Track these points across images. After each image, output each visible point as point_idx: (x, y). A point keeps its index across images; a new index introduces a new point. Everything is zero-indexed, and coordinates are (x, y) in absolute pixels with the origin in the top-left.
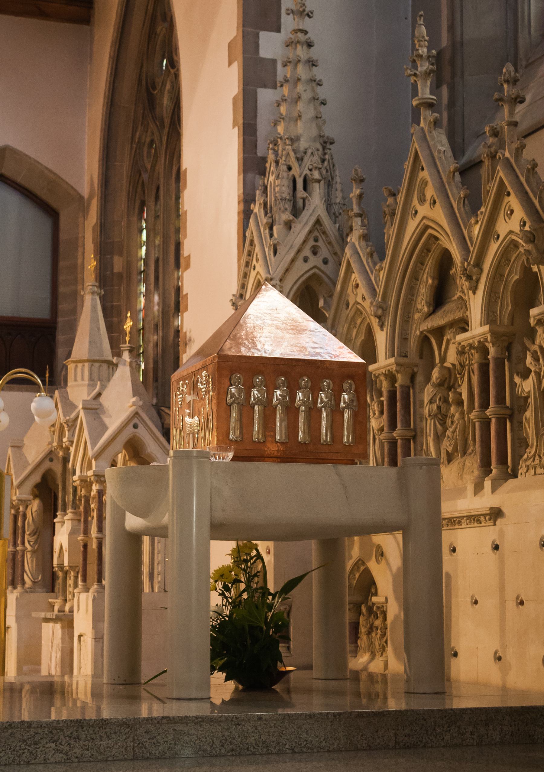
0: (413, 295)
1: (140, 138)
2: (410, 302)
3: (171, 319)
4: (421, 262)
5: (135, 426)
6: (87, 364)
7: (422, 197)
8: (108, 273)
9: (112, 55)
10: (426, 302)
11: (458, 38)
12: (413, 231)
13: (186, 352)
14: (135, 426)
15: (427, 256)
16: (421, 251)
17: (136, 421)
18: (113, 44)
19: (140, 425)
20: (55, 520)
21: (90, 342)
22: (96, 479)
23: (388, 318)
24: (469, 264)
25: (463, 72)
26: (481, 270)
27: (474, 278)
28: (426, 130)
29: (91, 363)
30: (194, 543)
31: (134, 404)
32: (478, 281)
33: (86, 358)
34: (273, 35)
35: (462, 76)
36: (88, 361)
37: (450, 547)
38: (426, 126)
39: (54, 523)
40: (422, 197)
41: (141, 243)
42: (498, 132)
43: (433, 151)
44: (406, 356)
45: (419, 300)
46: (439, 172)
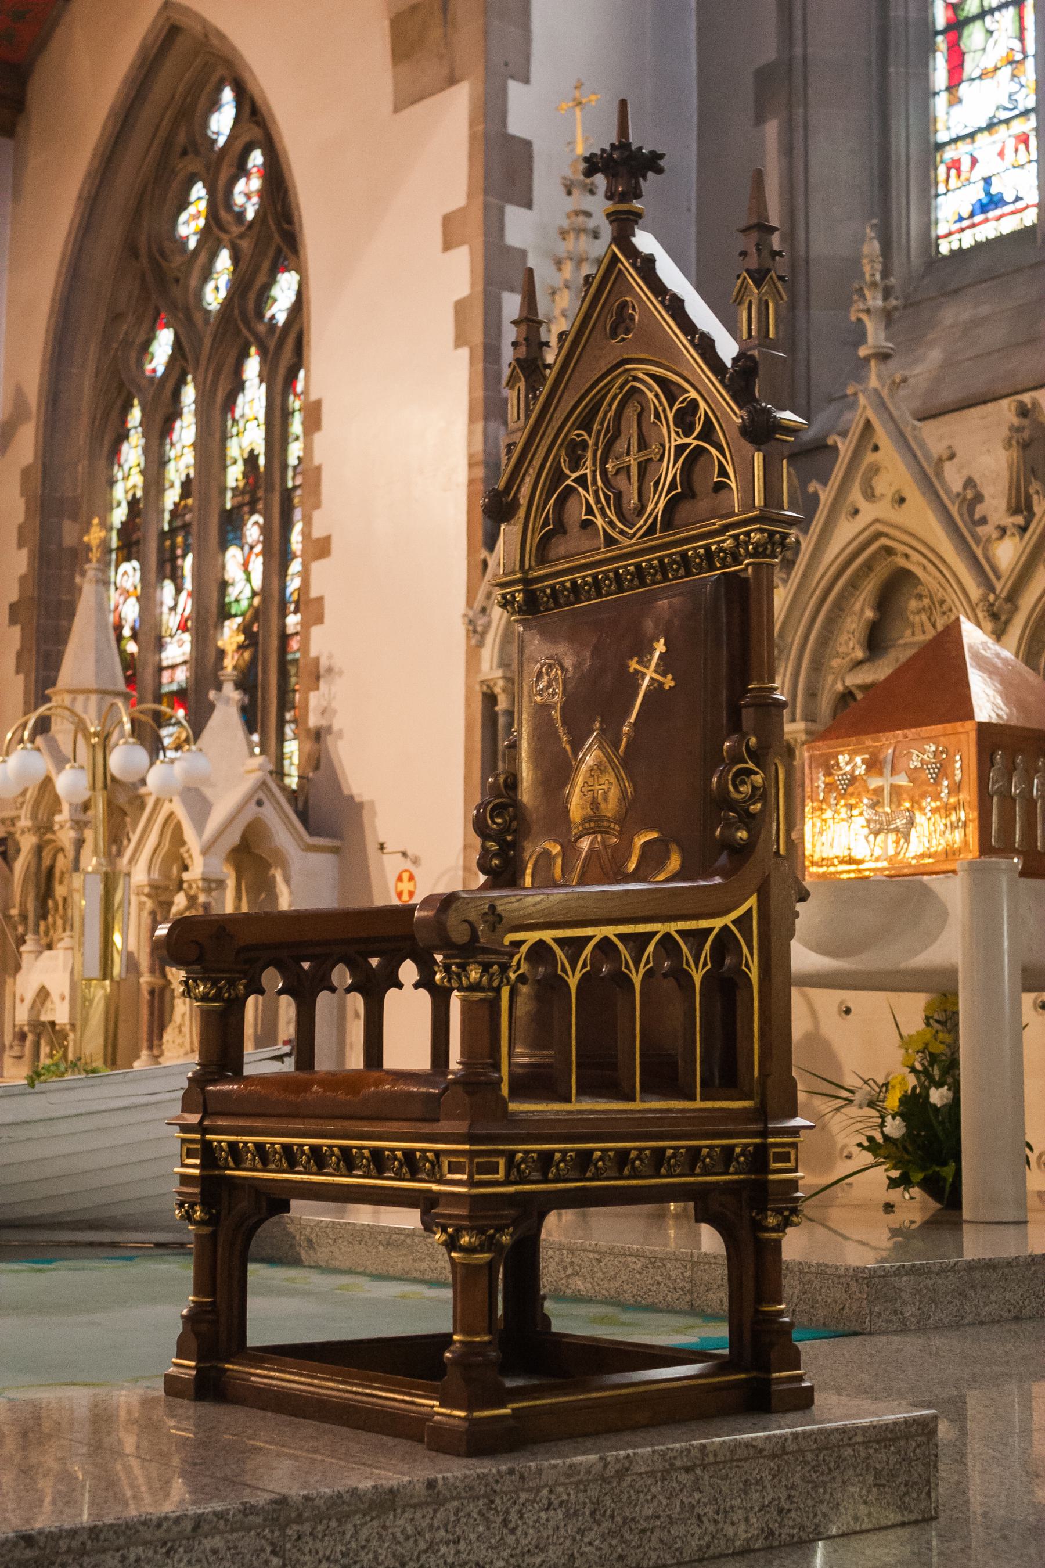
0: (832, 632)
1: (126, 333)
2: (825, 640)
3: (211, 631)
4: (854, 585)
5: (260, 803)
6: (94, 698)
7: (869, 491)
8: (54, 547)
9: (85, 194)
10: (858, 642)
11: (802, 253)
12: (848, 539)
13: (317, 688)
14: (260, 803)
15: (867, 576)
16: (859, 569)
17: (261, 795)
18: (90, 175)
19: (267, 803)
20: (23, 949)
21: (97, 662)
22: (206, 885)
23: (787, 663)
24: (997, 597)
25: (808, 301)
26: (1016, 609)
27: (1003, 618)
28: (885, 393)
29: (100, 696)
30: (1007, 991)
31: (261, 768)
32: (1007, 622)
33: (94, 686)
34: (523, 212)
35: (808, 308)
36: (98, 691)
37: (840, 1006)
38: (883, 386)
39: (20, 954)
40: (869, 491)
41: (111, 504)
42: (1028, 411)
43: (902, 426)
44: (814, 721)
45: (844, 638)
46: (915, 456)
